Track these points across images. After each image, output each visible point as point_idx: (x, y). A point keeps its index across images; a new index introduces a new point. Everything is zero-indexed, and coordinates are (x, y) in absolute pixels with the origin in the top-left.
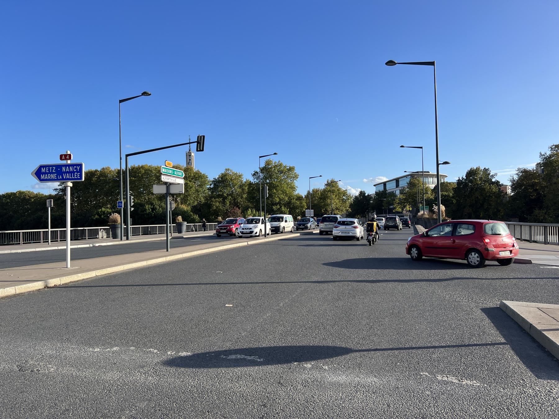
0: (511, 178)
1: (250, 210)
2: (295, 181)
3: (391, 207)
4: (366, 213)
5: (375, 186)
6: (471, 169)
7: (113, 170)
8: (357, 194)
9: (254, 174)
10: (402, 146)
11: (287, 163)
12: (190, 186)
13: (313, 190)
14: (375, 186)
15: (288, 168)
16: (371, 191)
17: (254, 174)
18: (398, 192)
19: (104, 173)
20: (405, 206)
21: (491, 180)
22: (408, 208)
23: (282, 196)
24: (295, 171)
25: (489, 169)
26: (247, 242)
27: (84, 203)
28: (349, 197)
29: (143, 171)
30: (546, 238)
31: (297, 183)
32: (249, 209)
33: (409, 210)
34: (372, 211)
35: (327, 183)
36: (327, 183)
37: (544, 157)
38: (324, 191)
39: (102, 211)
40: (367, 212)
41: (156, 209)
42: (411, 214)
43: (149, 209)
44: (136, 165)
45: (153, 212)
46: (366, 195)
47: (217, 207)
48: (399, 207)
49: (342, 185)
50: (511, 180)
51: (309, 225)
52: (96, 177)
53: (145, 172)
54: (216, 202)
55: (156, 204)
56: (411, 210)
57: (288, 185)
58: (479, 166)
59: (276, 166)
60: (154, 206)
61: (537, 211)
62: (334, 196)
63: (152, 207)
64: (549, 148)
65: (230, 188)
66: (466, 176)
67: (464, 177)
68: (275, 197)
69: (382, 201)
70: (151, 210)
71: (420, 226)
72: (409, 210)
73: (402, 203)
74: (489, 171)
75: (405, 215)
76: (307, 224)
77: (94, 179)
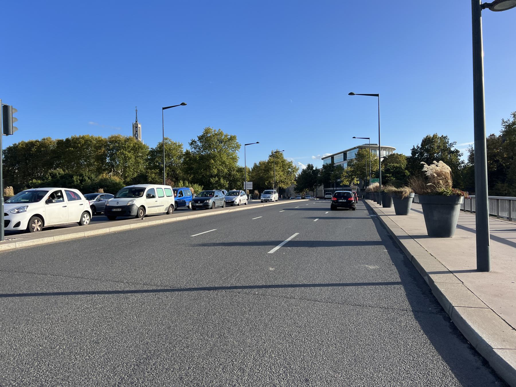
0: (470, 147)
1: (181, 182)
2: (237, 151)
3: (339, 180)
4: (314, 186)
5: (323, 159)
6: (427, 136)
7: (54, 140)
8: (305, 167)
9: (191, 143)
10: (351, 94)
11: (228, 132)
12: (128, 156)
13: (260, 163)
14: (323, 159)
15: (230, 136)
16: (319, 165)
17: (192, 144)
18: (345, 166)
19: (45, 143)
20: (353, 179)
21: (450, 148)
22: (356, 181)
23: (221, 168)
24: (237, 141)
25: (447, 136)
26: (263, 205)
27: (22, 174)
28: (296, 169)
29: (83, 142)
30: (510, 214)
31: (239, 154)
32: (181, 181)
33: (357, 184)
34: (319, 185)
35: (271, 154)
36: (271, 154)
37: (506, 124)
38: (268, 162)
39: (32, 182)
40: (314, 186)
41: (85, 180)
42: (359, 188)
43: (77, 181)
44: (78, 136)
45: (82, 184)
46: (314, 169)
47: (153, 179)
48: (346, 180)
49: (288, 158)
50: (470, 150)
51: (210, 202)
52: (36, 148)
53: (85, 143)
54: (152, 173)
55: (86, 175)
56: (359, 183)
57: (228, 156)
58: (436, 133)
59: (216, 134)
60: (83, 177)
61: (500, 185)
62: (278, 168)
63: (81, 178)
64: (511, 114)
65: (167, 158)
66: (421, 145)
67: (420, 146)
68: (213, 167)
69: (329, 175)
70: (79, 182)
71: (370, 201)
72: (357, 184)
73: (350, 176)
74: (447, 139)
75: (352, 189)
76: (207, 200)
77: (33, 150)
